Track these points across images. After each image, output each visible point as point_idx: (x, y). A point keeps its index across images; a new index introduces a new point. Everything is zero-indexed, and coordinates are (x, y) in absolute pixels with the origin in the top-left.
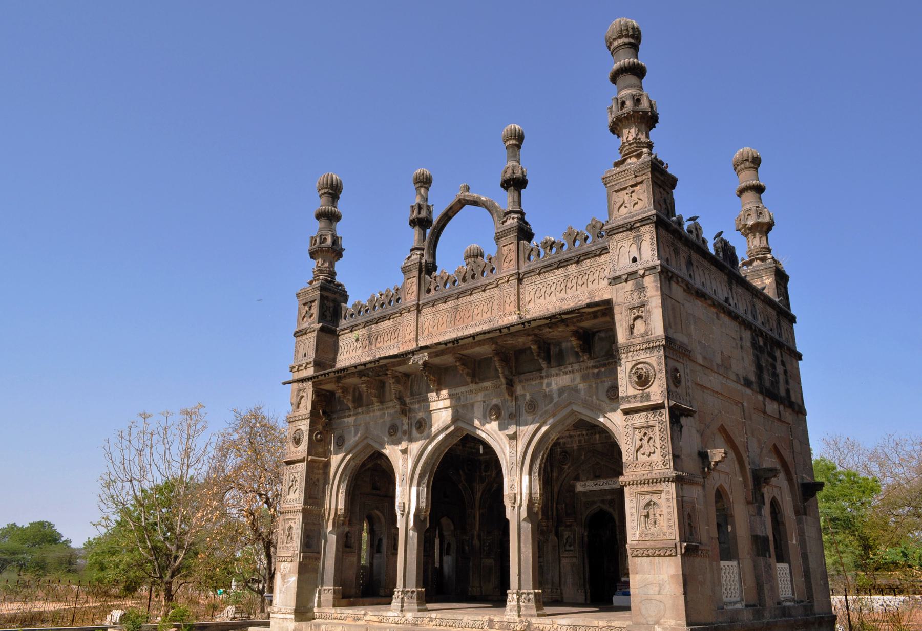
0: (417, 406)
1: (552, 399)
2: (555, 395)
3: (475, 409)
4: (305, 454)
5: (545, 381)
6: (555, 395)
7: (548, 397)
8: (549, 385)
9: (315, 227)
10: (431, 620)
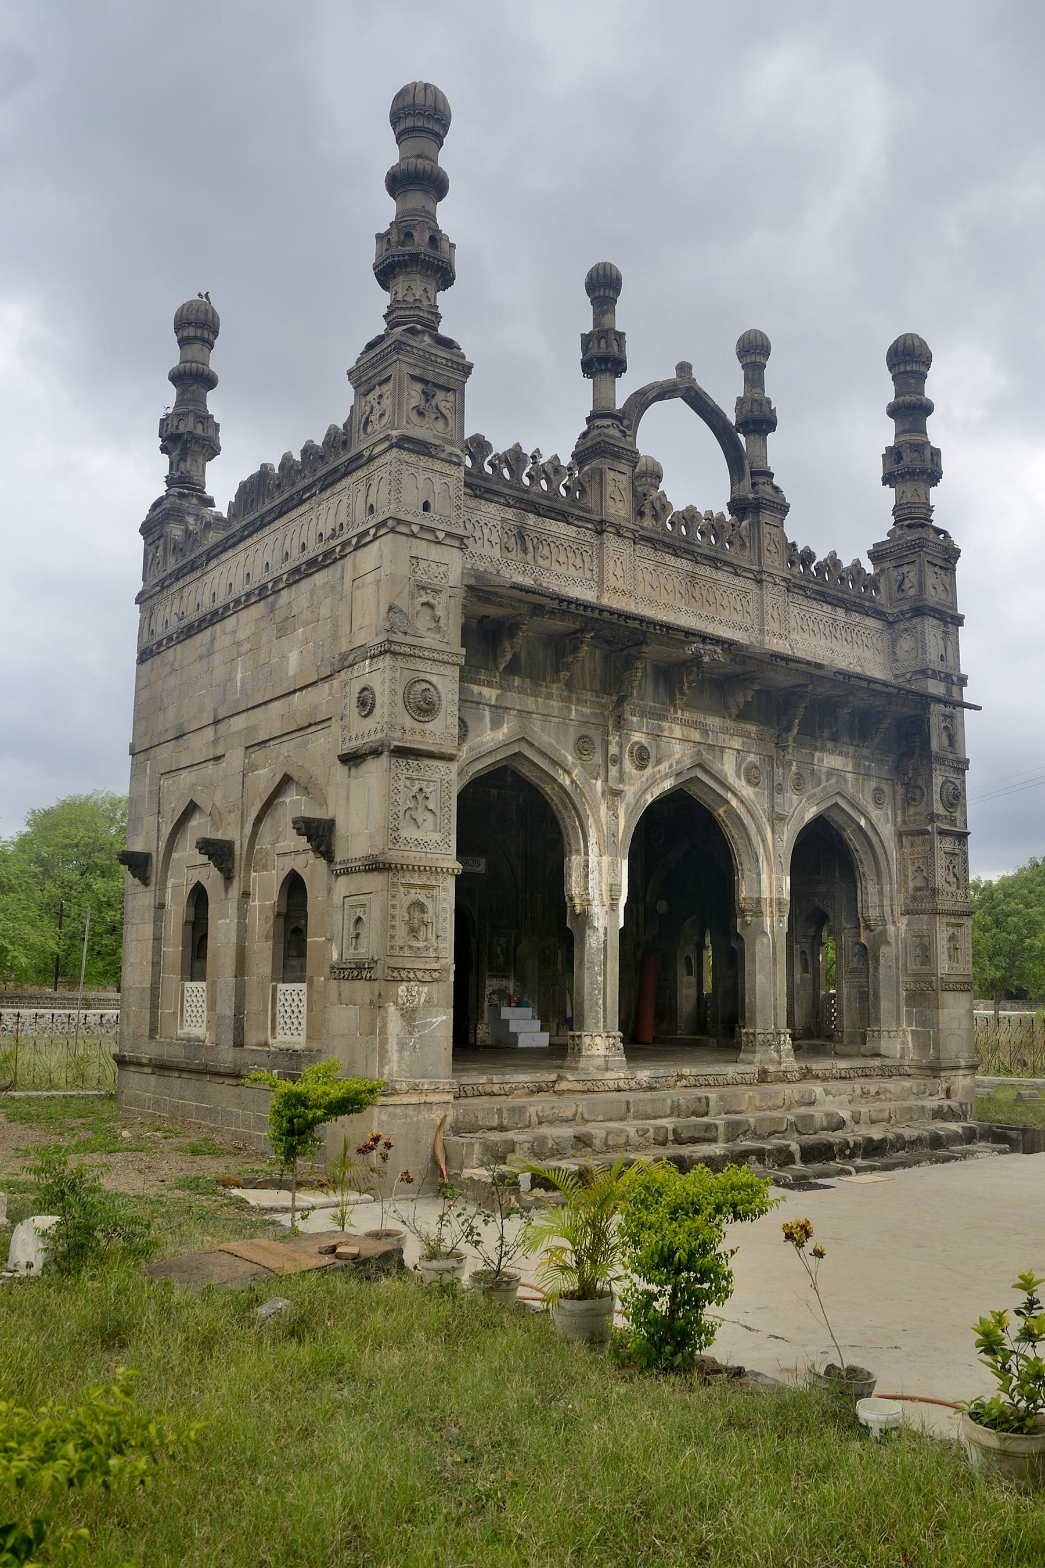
5: (817, 754)
10: (681, 1077)
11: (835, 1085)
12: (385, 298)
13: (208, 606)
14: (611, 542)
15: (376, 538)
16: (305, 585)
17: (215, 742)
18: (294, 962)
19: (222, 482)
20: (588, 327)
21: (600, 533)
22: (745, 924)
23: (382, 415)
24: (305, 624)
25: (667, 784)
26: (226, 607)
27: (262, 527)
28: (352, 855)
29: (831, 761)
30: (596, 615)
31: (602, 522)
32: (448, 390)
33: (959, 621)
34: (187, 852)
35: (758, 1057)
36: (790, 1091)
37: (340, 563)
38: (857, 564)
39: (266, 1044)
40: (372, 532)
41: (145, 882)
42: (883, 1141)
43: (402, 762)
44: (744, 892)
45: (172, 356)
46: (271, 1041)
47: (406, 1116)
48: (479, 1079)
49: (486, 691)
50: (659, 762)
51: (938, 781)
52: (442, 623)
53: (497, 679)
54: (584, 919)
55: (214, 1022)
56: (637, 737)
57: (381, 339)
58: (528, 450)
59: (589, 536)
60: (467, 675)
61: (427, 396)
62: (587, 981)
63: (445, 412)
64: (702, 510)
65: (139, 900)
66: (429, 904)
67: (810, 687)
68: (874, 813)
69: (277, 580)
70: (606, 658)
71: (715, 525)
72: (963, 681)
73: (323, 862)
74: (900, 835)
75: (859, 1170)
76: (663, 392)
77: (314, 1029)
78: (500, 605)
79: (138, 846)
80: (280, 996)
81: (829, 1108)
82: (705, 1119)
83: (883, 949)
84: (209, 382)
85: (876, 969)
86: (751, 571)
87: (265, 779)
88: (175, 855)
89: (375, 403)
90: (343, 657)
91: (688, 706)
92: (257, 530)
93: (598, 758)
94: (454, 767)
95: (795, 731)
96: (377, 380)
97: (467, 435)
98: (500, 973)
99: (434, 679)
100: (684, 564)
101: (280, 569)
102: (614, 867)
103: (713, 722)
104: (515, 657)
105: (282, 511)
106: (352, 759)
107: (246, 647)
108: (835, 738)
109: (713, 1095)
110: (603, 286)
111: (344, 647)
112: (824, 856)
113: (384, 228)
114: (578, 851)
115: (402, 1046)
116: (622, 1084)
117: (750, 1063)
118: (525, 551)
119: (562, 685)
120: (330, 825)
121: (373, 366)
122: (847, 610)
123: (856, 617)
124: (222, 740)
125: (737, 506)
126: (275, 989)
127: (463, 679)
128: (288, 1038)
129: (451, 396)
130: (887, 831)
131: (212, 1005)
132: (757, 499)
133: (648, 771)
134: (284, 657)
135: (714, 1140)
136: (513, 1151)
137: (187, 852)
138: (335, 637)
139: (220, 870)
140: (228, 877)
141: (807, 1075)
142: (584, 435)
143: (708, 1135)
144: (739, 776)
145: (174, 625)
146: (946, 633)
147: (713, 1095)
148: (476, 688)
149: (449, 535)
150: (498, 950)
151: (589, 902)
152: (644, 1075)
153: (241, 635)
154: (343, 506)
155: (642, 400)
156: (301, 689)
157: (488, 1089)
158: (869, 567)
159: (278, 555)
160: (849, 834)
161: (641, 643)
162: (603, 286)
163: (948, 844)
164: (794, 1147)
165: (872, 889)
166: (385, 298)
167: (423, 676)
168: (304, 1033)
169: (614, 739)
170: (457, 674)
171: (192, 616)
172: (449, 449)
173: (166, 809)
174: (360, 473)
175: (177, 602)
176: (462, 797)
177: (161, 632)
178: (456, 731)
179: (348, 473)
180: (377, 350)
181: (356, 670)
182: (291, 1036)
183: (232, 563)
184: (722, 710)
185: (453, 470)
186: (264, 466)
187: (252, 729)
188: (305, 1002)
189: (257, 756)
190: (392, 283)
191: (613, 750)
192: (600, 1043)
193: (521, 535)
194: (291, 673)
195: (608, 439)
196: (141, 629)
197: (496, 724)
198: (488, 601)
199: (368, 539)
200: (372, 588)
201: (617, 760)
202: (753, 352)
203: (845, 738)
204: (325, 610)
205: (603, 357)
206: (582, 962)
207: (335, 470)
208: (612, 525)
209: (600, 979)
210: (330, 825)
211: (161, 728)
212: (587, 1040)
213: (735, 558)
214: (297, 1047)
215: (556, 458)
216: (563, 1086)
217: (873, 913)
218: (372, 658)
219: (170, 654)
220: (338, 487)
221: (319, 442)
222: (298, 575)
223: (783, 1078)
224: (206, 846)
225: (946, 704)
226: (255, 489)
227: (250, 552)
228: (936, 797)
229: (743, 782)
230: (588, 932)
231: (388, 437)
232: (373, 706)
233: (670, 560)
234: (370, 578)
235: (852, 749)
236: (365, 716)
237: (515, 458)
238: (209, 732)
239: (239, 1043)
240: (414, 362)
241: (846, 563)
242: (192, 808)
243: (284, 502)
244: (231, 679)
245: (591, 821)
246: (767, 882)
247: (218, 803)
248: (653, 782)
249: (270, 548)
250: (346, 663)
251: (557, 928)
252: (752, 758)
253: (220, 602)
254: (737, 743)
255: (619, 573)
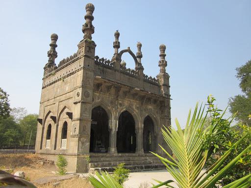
13: (54, 80)
14: (117, 72)
19: (57, 61)
25: (124, 109)
29: (150, 107)
33: (170, 87)
34: (49, 119)
36: (143, 158)
38: (154, 78)
41: (41, 124)
44: (136, 127)
45: (50, 42)
54: (111, 130)
55: (51, 146)
61: (90, 49)
64: (131, 69)
65: (40, 126)
70: (116, 90)
71: (133, 71)
72: (170, 96)
74: (161, 118)
77: (67, 146)
79: (40, 118)
84: (56, 46)
87: (62, 107)
91: (128, 98)
98: (99, 140)
100: (128, 76)
101: (66, 75)
104: (102, 89)
106: (75, 103)
109: (131, 158)
110: (117, 35)
111: (75, 86)
113: (84, 24)
115: (81, 148)
130: (159, 118)
131: (51, 144)
132: (140, 68)
137: (49, 119)
138: (74, 85)
140: (55, 122)
152: (120, 154)
155: (122, 52)
158: (156, 79)
159: (66, 72)
162: (117, 35)
163: (168, 120)
164: (143, 166)
165: (156, 127)
169: (116, 102)
171: (51, 82)
177: (46, 84)
179: (77, 60)
182: (64, 148)
185: (93, 61)
187: (60, 99)
189: (61, 103)
195: (118, 56)
197: (98, 99)
202: (140, 46)
203: (152, 103)
205: (117, 46)
213: (156, 163)
217: (157, 131)
219: (47, 88)
222: (68, 76)
223: (142, 156)
224: (52, 117)
237: (103, 59)
239: (55, 149)
240: (90, 46)
241: (153, 78)
242: (50, 112)
244: (57, 91)
246: (140, 125)
250: (75, 89)
254: (135, 104)
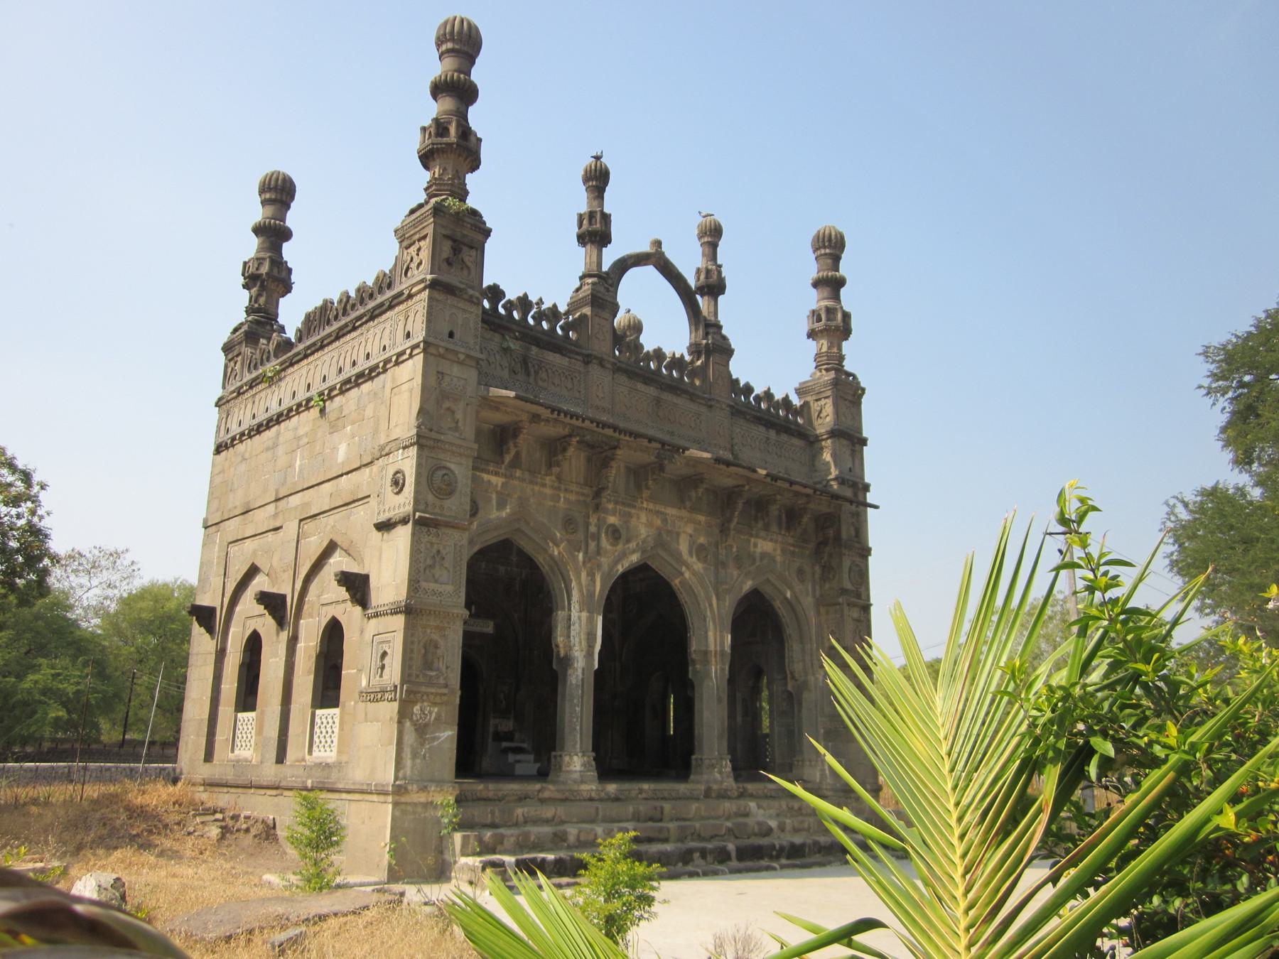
0: (610, 506)
1: (754, 560)
2: (758, 559)
3: (681, 540)
4: (409, 508)
5: (753, 540)
6: (758, 559)
7: (752, 558)
8: (755, 545)
9: (430, 110)
10: (641, 791)
11: (764, 803)
12: (427, 176)
14: (595, 370)
15: (411, 356)
16: (354, 393)
17: (276, 515)
18: (330, 693)
20: (584, 209)
21: (587, 363)
22: (696, 672)
23: (420, 263)
24: (353, 423)
25: (635, 558)
26: (290, 410)
27: (322, 347)
28: (381, 602)
29: (763, 545)
30: (579, 423)
31: (588, 356)
32: (472, 248)
35: (705, 777)
36: (728, 806)
37: (382, 376)
39: (304, 760)
40: (408, 351)
42: (803, 845)
43: (425, 529)
44: (694, 646)
45: (257, 213)
46: (307, 757)
47: (414, 813)
48: (479, 787)
49: (494, 479)
50: (628, 541)
51: (847, 563)
52: (460, 424)
53: (502, 471)
54: (567, 661)
55: (260, 746)
56: (612, 520)
57: (421, 206)
58: (533, 298)
59: (579, 366)
60: (479, 464)
62: (567, 710)
63: (469, 264)
65: (202, 643)
66: (441, 643)
67: (747, 487)
68: (798, 587)
69: (332, 389)
70: (589, 460)
71: (677, 363)
72: (866, 488)
73: (359, 608)
75: (782, 867)
76: (638, 260)
78: (506, 412)
79: (204, 600)
80: (317, 720)
81: (760, 819)
82: (659, 824)
83: (805, 695)
85: (800, 711)
86: (703, 398)
88: (238, 609)
89: (414, 254)
90: (382, 448)
91: (652, 499)
92: (317, 350)
93: (580, 535)
94: (466, 535)
95: (736, 520)
96: (417, 236)
97: (485, 285)
99: (452, 466)
100: (652, 391)
102: (591, 621)
103: (671, 511)
104: (517, 455)
105: (338, 336)
106: (385, 526)
107: (305, 440)
108: (766, 528)
109: (667, 806)
111: (383, 440)
112: (757, 623)
114: (563, 609)
116: (593, 795)
117: (698, 782)
118: (528, 374)
119: (553, 478)
120: (365, 579)
121: (415, 226)
122: (778, 432)
123: (784, 437)
124: (281, 516)
125: (695, 349)
126: (313, 715)
127: (475, 468)
128: (322, 754)
129: (473, 253)
130: (808, 602)
131: (260, 731)
132: (712, 345)
133: (620, 547)
134: (335, 449)
135: (666, 840)
136: (502, 843)
137: (248, 604)
138: (376, 432)
139: (274, 617)
141: (742, 795)
142: (577, 290)
143: (662, 836)
144: (691, 554)
145: (248, 423)
146: (853, 451)
147: (667, 806)
148: (486, 477)
149: (468, 356)
150: (502, 696)
151: (571, 648)
152: (612, 788)
153: (301, 432)
154: (387, 332)
155: (624, 265)
156: (347, 473)
157: (484, 795)
160: (777, 604)
161: (615, 448)
163: (855, 613)
164: (731, 847)
165: (796, 647)
166: (427, 176)
167: (444, 463)
168: (335, 750)
169: (593, 520)
170: (471, 464)
171: (262, 417)
172: (471, 292)
173: (231, 571)
174: (401, 307)
175: (249, 406)
176: (472, 564)
177: (235, 430)
178: (468, 507)
179: (391, 307)
180: (418, 214)
181: (391, 458)
182: (325, 753)
183: (296, 376)
184: (681, 502)
186: (326, 302)
187: (306, 505)
188: (337, 724)
189: (308, 526)
190: (432, 164)
191: (593, 529)
192: (576, 763)
193: (525, 361)
194: (340, 461)
196: (219, 427)
197: (501, 505)
198: (497, 409)
199: (406, 356)
200: (406, 395)
201: (597, 538)
202: (712, 235)
203: (774, 528)
204: (369, 412)
205: (595, 232)
206: (564, 696)
207: (382, 304)
208: (596, 358)
209: (578, 709)
210: (365, 579)
211: (231, 505)
212: (567, 759)
214: (329, 761)
215: (555, 306)
216: (546, 794)
217: (798, 667)
218: (404, 448)
220: (384, 317)
221: (370, 283)
223: (723, 795)
225: (851, 502)
226: (319, 317)
227: (312, 367)
228: (846, 576)
229: (694, 559)
230: (570, 671)
231: (422, 281)
232: (403, 485)
233: (641, 386)
234: (405, 387)
235: (780, 538)
236: (398, 493)
237: (524, 303)
238: (271, 508)
239: (281, 758)
243: (341, 329)
244: (291, 466)
245: (574, 584)
246: (712, 639)
247: (275, 564)
248: (624, 555)
249: (327, 364)
250: (384, 453)
251: (545, 669)
252: (702, 540)
253: (285, 406)
255: (601, 395)
